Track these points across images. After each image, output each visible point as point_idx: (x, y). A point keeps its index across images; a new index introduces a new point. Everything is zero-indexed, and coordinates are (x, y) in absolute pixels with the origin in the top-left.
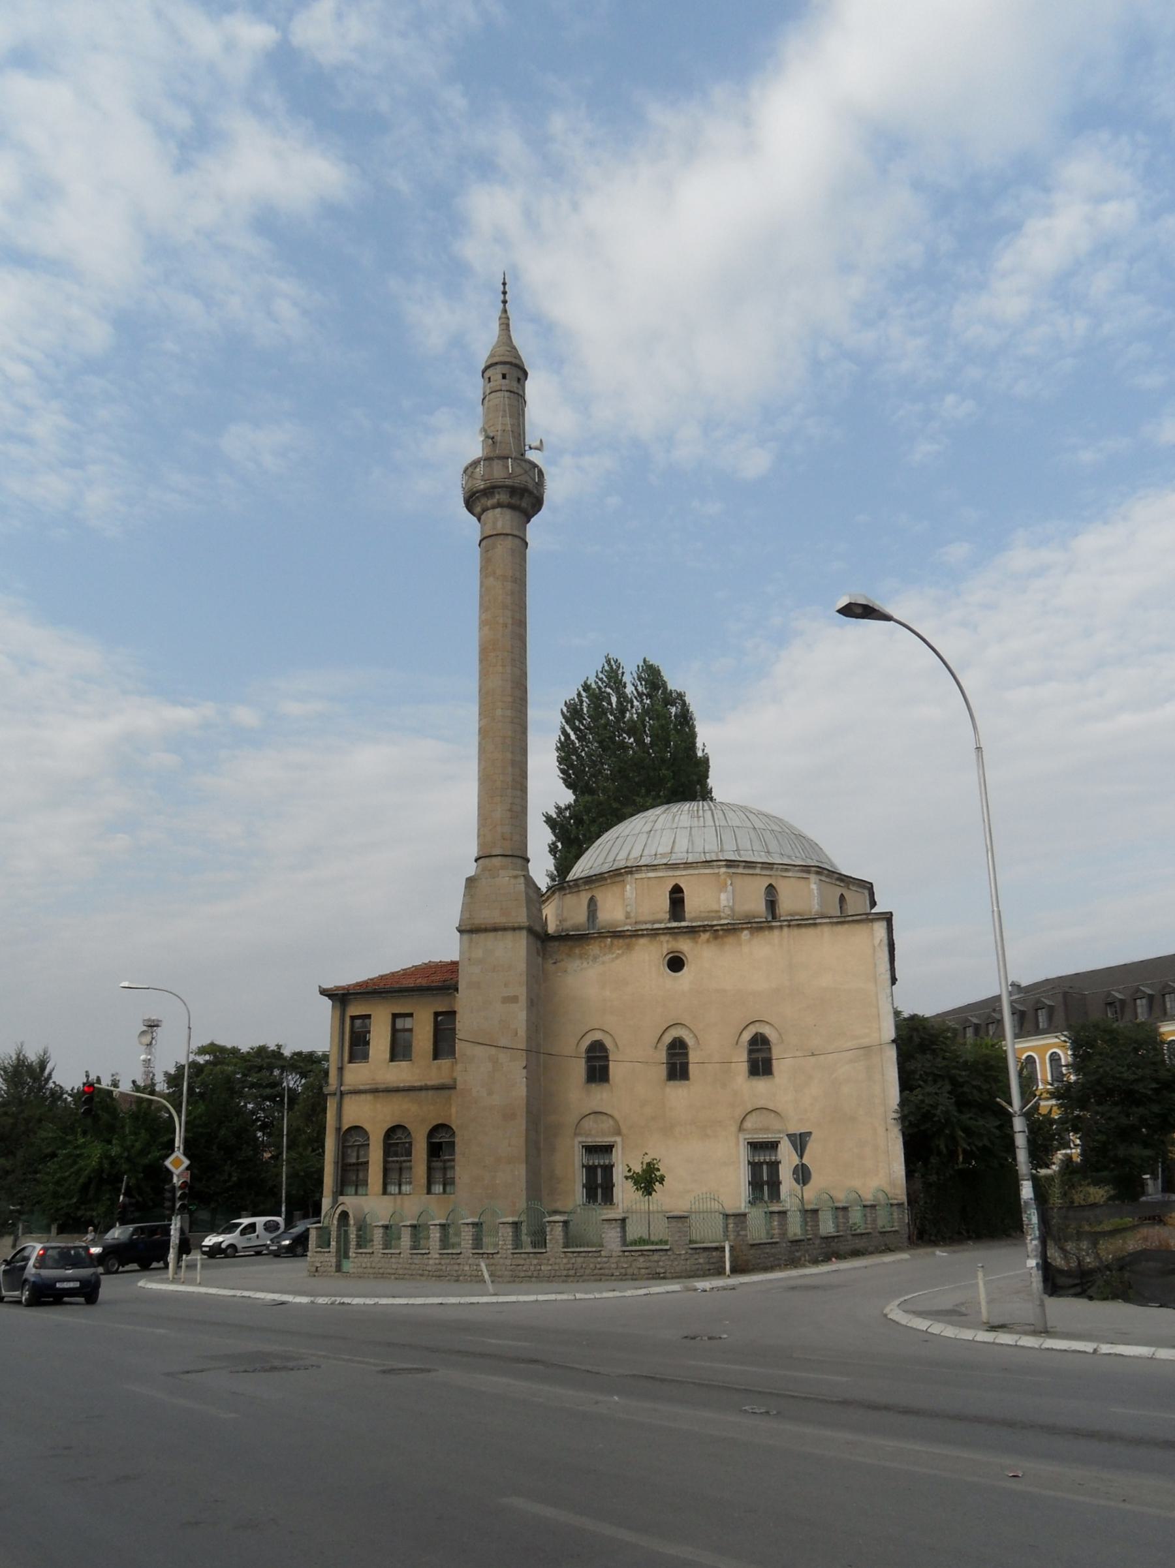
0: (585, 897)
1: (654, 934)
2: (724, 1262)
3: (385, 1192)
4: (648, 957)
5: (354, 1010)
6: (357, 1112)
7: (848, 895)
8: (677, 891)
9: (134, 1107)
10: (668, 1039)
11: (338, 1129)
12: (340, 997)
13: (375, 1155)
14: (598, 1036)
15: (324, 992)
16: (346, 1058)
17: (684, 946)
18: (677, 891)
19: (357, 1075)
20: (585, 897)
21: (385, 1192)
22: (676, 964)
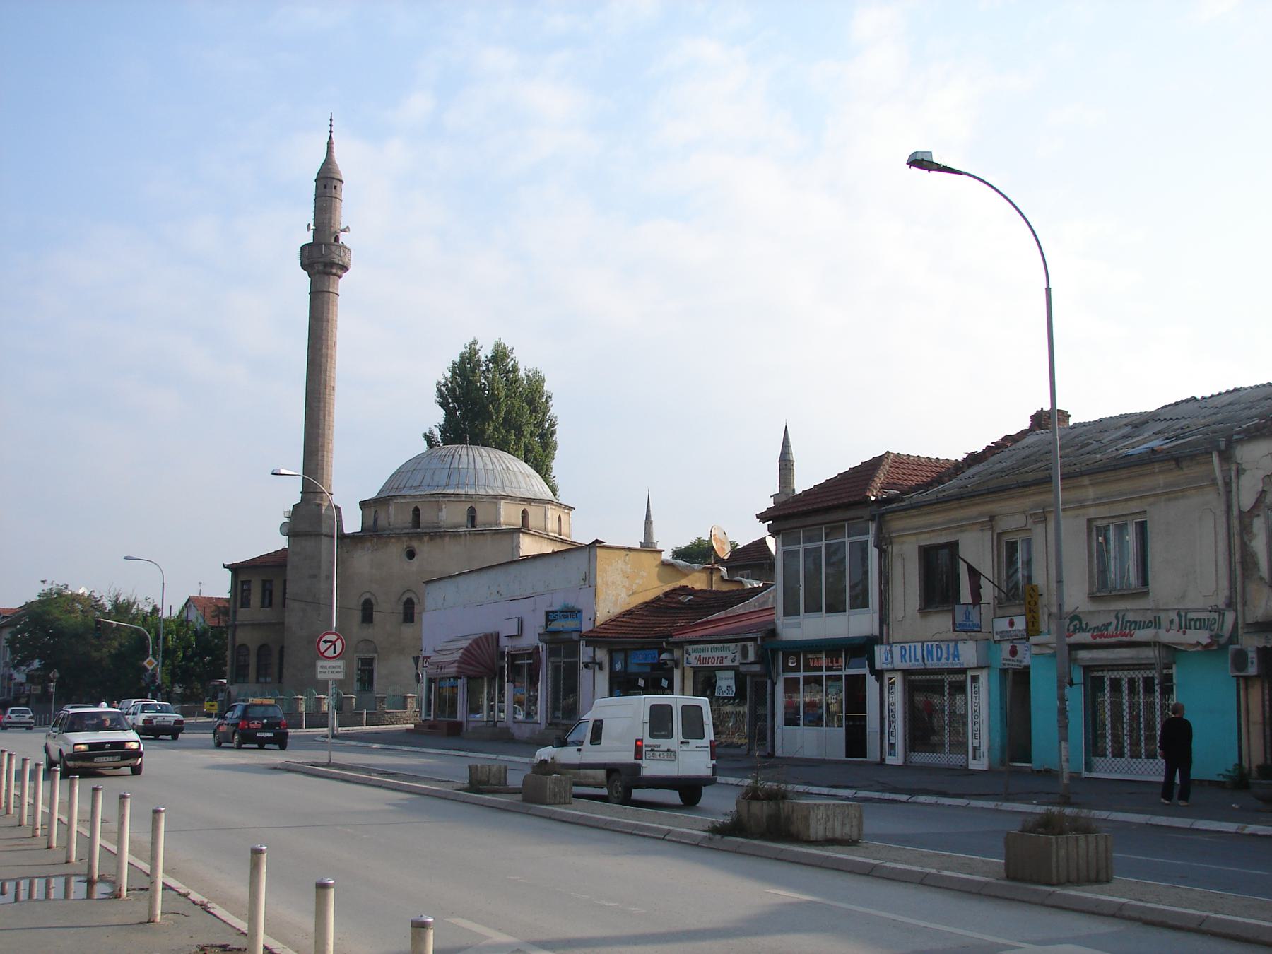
0: (373, 510)
1: (399, 536)
2: (973, 881)
3: (258, 681)
4: (395, 551)
5: (242, 578)
6: (243, 636)
7: (529, 508)
8: (416, 510)
9: (149, 609)
10: (404, 598)
11: (234, 646)
12: (235, 569)
13: (253, 661)
14: (368, 596)
15: (225, 566)
16: (238, 604)
17: (415, 544)
18: (416, 510)
19: (243, 615)
20: (373, 510)
21: (258, 681)
22: (411, 554)
